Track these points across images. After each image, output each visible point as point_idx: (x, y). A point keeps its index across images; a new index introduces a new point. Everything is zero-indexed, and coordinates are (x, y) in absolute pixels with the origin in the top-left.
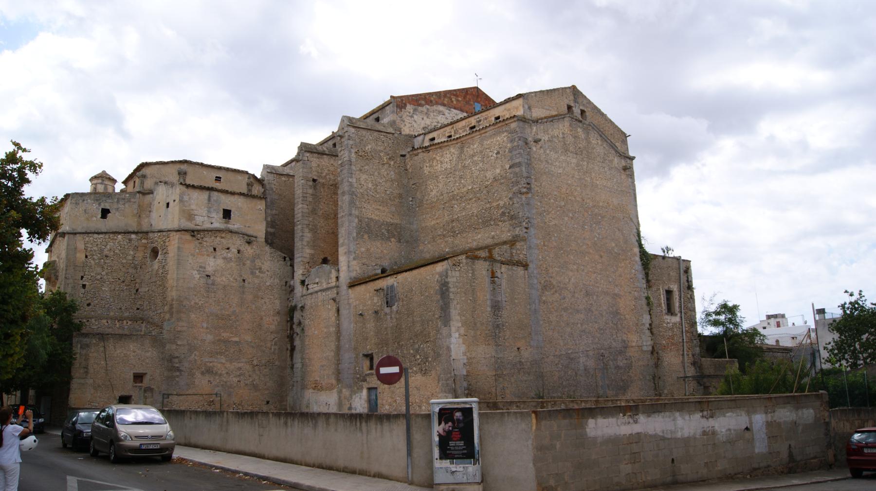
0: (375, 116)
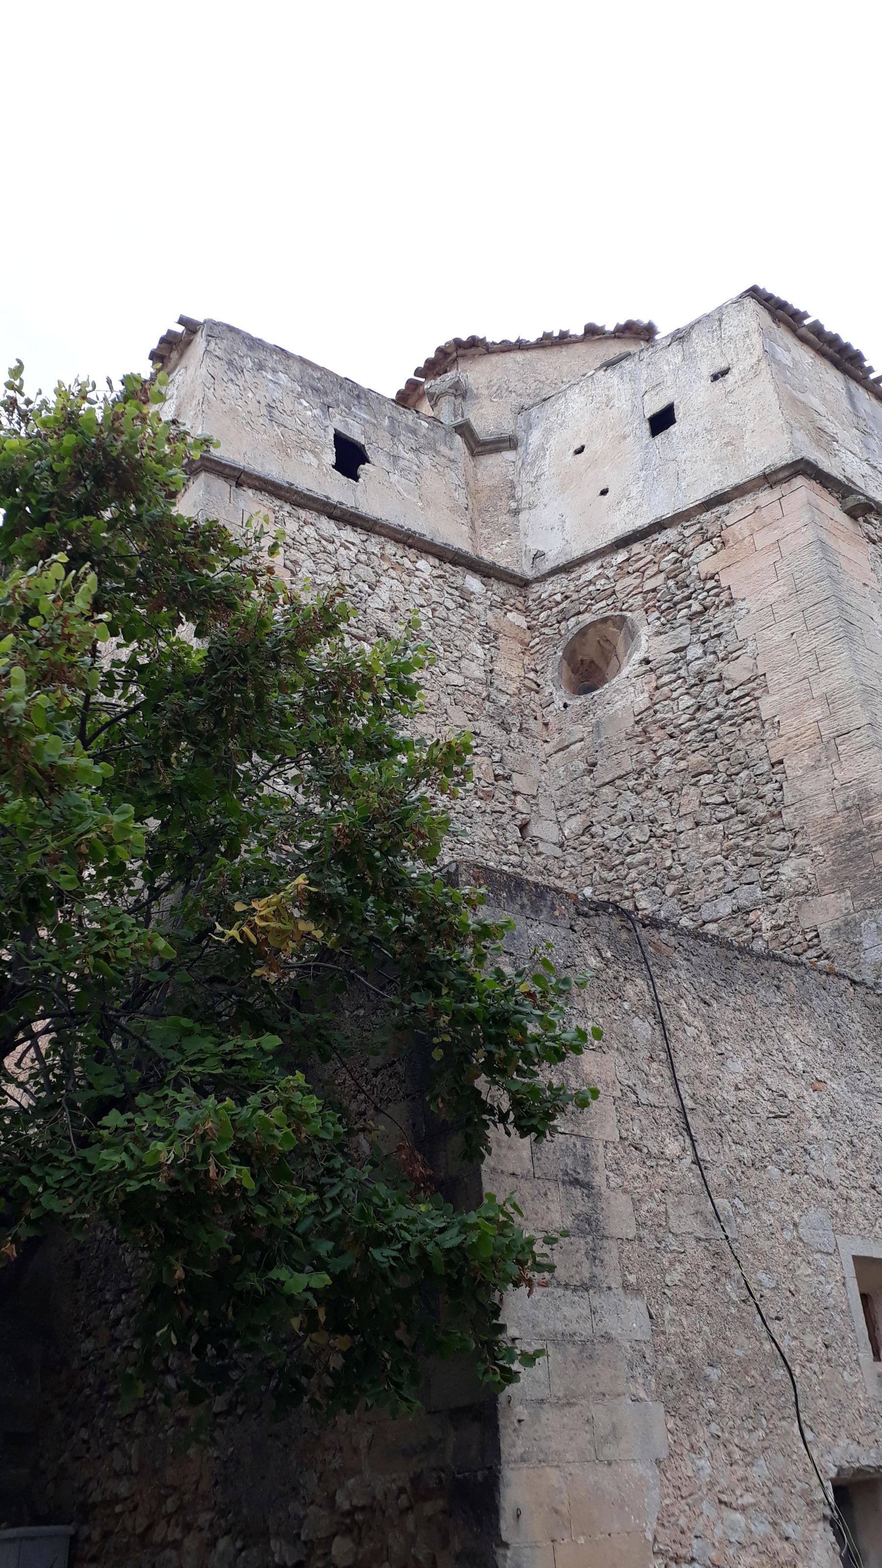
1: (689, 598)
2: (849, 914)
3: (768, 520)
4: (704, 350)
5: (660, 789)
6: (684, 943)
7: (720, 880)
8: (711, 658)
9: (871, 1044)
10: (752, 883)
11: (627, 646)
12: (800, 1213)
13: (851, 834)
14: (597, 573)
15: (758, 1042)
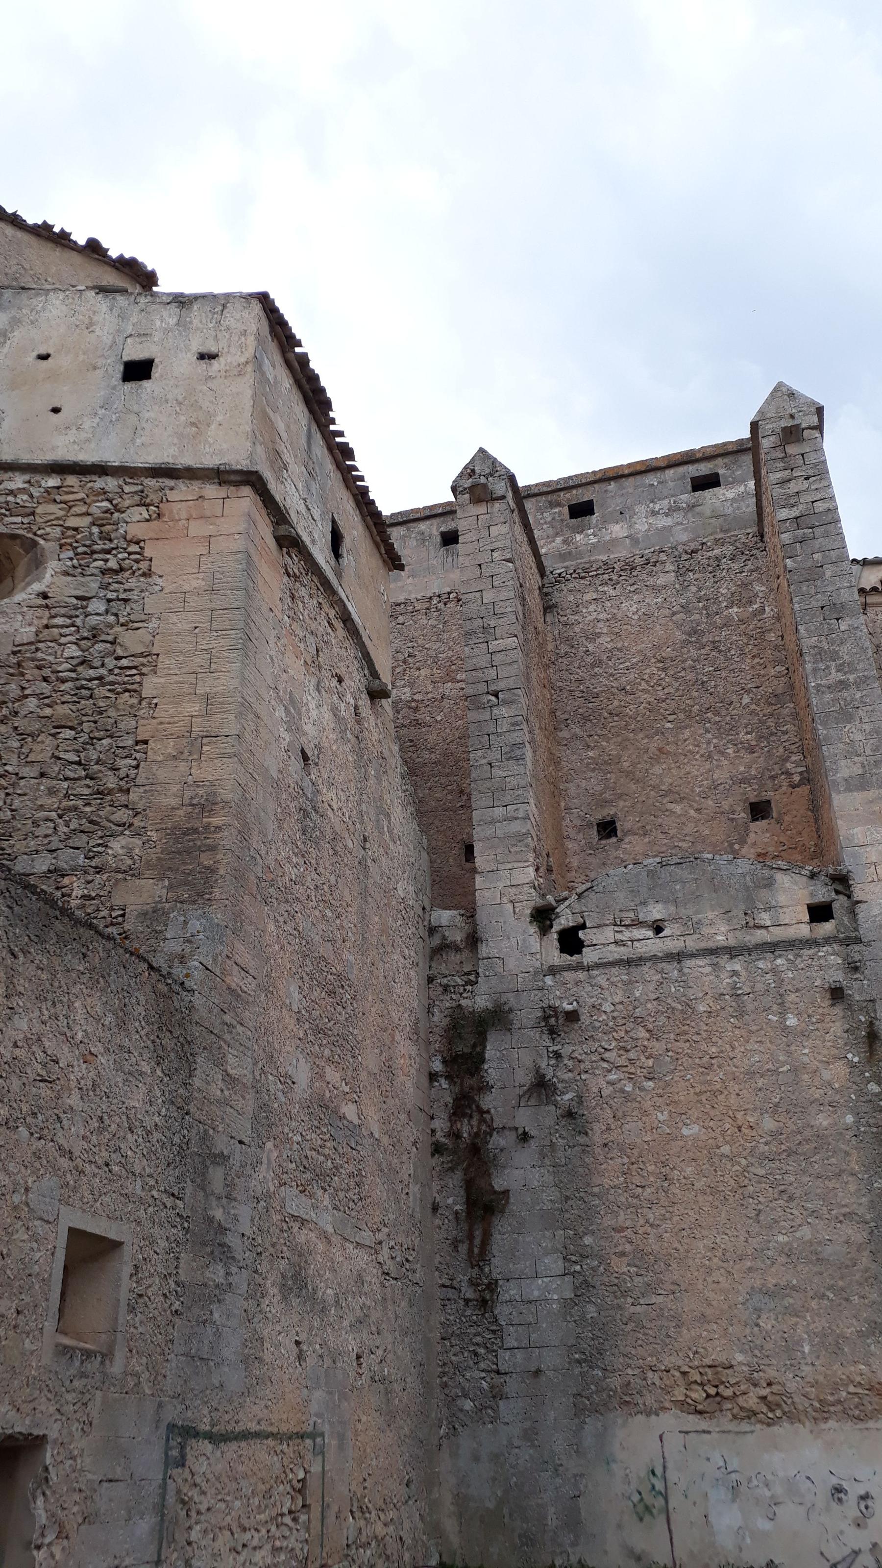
0: (703, 469)
1: (108, 552)
2: (160, 902)
3: (208, 513)
4: (200, 325)
5: (16, 728)
6: (12, 889)
7: (46, 836)
8: (111, 619)
9: (147, 1029)
10: (78, 849)
11: (28, 573)
12: (35, 1178)
13: (188, 829)
14: (21, 486)
15: (49, 1003)
